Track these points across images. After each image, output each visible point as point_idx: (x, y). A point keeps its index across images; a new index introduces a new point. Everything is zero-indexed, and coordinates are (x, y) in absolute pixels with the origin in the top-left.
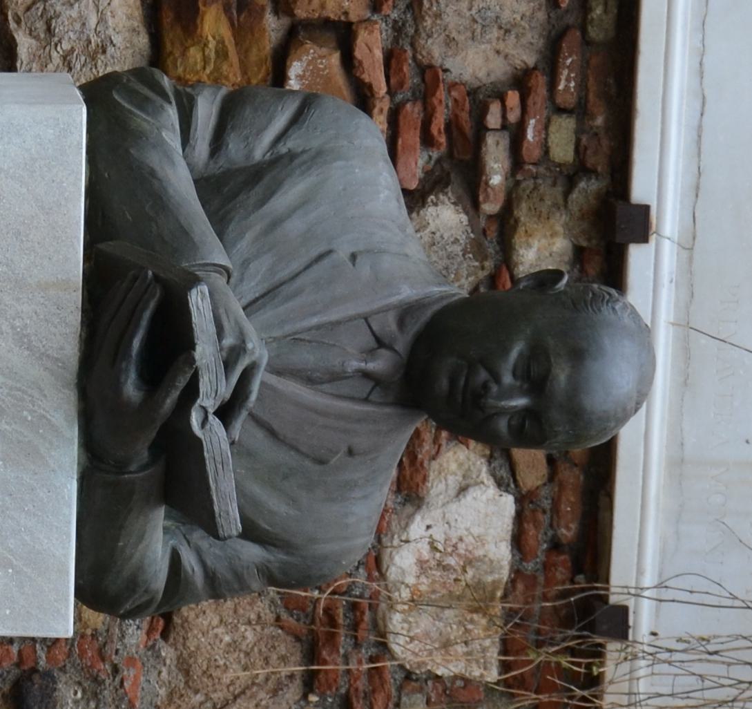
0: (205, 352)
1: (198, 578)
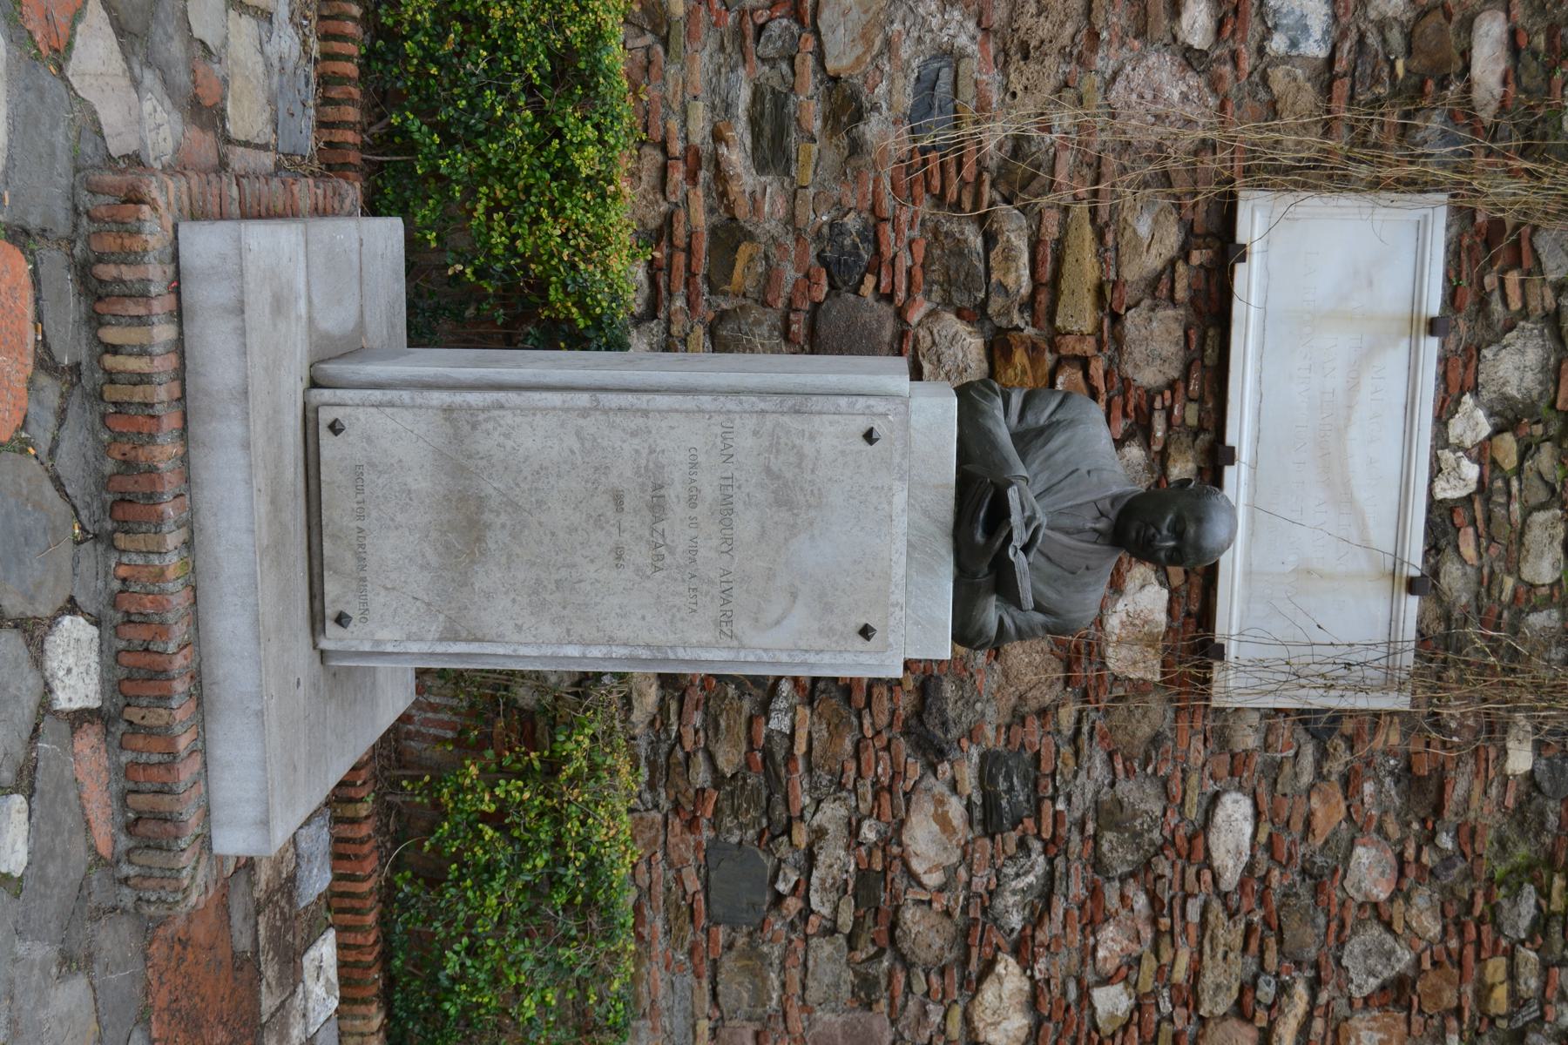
0: (1016, 519)
1: (1012, 630)
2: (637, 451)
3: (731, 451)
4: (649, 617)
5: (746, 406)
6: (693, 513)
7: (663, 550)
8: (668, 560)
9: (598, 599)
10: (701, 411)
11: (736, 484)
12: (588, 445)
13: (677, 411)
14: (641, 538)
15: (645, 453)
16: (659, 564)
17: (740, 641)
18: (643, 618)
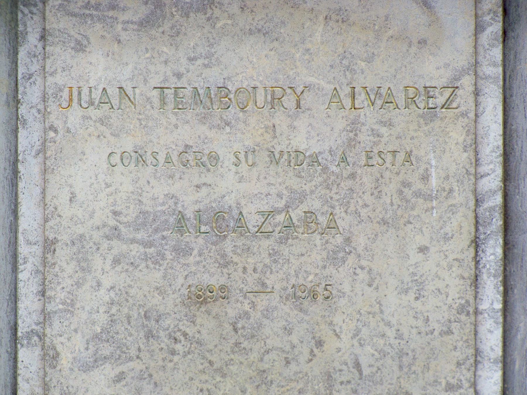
2: (116, 261)
3: (113, 92)
4: (421, 240)
5: (35, 67)
6: (228, 160)
7: (296, 214)
8: (315, 204)
9: (391, 333)
10: (43, 150)
11: (173, 82)
12: (106, 350)
13: (44, 192)
14: (274, 254)
15: (118, 247)
16: (323, 220)
17: (463, 72)
18: (423, 250)
